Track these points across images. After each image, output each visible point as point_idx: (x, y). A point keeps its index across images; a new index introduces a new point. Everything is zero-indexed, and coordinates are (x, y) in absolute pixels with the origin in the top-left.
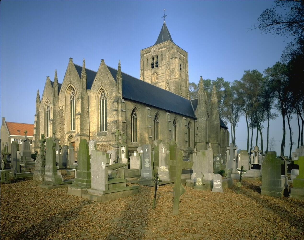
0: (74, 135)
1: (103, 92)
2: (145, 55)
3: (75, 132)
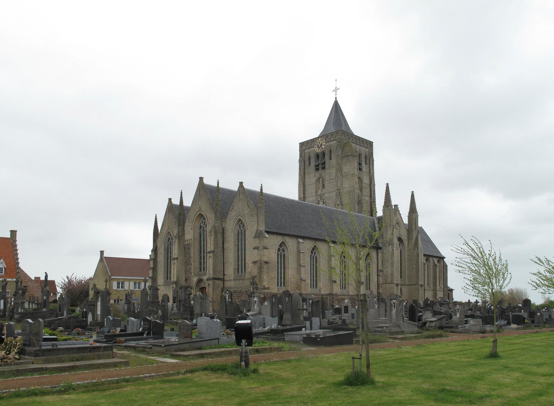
0: (205, 278)
1: (241, 223)
2: (306, 151)
3: (205, 275)
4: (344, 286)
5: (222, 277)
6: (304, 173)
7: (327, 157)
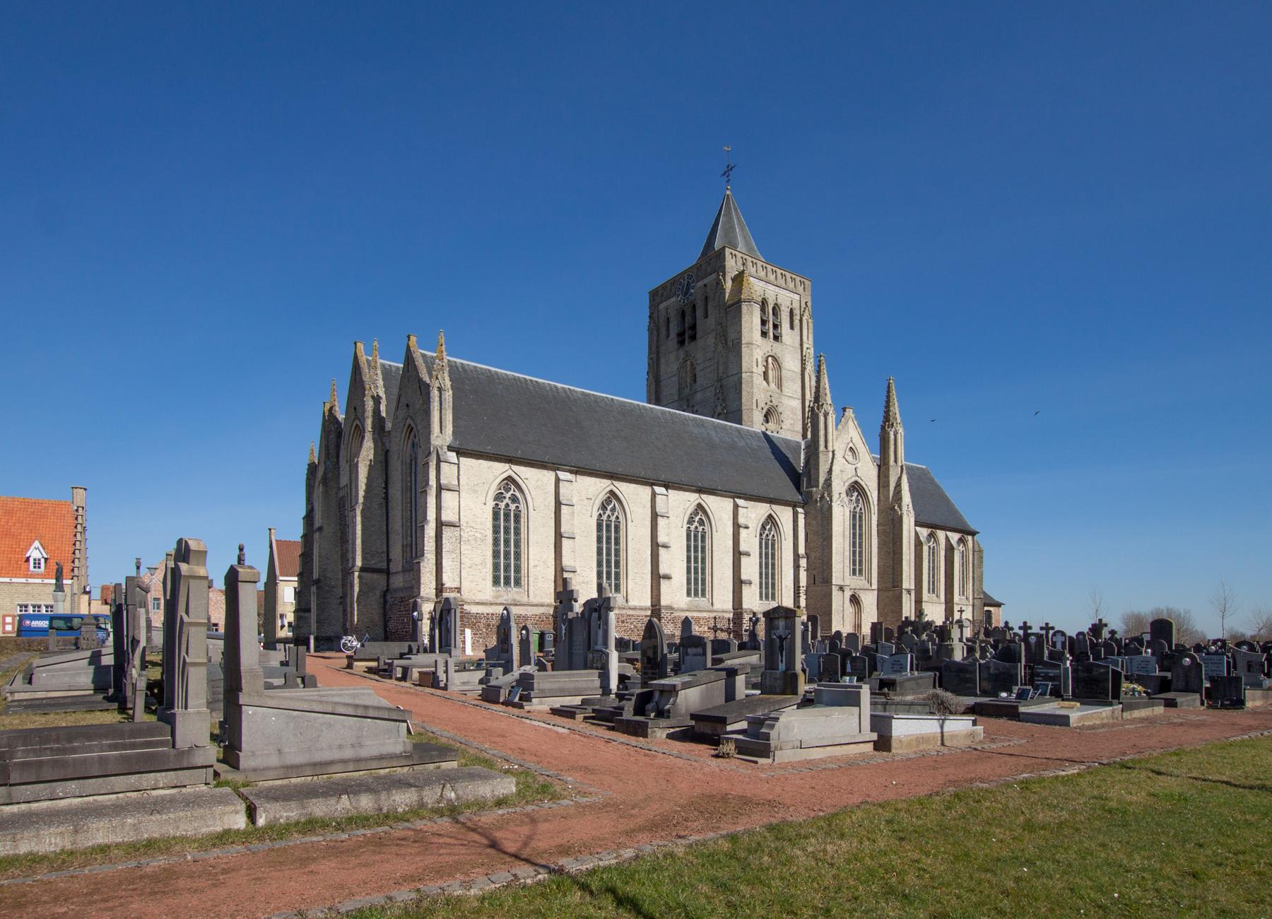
4: (698, 582)
5: (384, 566)
6: (658, 353)
7: (699, 313)
